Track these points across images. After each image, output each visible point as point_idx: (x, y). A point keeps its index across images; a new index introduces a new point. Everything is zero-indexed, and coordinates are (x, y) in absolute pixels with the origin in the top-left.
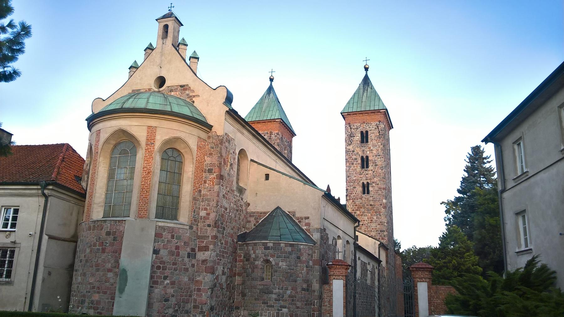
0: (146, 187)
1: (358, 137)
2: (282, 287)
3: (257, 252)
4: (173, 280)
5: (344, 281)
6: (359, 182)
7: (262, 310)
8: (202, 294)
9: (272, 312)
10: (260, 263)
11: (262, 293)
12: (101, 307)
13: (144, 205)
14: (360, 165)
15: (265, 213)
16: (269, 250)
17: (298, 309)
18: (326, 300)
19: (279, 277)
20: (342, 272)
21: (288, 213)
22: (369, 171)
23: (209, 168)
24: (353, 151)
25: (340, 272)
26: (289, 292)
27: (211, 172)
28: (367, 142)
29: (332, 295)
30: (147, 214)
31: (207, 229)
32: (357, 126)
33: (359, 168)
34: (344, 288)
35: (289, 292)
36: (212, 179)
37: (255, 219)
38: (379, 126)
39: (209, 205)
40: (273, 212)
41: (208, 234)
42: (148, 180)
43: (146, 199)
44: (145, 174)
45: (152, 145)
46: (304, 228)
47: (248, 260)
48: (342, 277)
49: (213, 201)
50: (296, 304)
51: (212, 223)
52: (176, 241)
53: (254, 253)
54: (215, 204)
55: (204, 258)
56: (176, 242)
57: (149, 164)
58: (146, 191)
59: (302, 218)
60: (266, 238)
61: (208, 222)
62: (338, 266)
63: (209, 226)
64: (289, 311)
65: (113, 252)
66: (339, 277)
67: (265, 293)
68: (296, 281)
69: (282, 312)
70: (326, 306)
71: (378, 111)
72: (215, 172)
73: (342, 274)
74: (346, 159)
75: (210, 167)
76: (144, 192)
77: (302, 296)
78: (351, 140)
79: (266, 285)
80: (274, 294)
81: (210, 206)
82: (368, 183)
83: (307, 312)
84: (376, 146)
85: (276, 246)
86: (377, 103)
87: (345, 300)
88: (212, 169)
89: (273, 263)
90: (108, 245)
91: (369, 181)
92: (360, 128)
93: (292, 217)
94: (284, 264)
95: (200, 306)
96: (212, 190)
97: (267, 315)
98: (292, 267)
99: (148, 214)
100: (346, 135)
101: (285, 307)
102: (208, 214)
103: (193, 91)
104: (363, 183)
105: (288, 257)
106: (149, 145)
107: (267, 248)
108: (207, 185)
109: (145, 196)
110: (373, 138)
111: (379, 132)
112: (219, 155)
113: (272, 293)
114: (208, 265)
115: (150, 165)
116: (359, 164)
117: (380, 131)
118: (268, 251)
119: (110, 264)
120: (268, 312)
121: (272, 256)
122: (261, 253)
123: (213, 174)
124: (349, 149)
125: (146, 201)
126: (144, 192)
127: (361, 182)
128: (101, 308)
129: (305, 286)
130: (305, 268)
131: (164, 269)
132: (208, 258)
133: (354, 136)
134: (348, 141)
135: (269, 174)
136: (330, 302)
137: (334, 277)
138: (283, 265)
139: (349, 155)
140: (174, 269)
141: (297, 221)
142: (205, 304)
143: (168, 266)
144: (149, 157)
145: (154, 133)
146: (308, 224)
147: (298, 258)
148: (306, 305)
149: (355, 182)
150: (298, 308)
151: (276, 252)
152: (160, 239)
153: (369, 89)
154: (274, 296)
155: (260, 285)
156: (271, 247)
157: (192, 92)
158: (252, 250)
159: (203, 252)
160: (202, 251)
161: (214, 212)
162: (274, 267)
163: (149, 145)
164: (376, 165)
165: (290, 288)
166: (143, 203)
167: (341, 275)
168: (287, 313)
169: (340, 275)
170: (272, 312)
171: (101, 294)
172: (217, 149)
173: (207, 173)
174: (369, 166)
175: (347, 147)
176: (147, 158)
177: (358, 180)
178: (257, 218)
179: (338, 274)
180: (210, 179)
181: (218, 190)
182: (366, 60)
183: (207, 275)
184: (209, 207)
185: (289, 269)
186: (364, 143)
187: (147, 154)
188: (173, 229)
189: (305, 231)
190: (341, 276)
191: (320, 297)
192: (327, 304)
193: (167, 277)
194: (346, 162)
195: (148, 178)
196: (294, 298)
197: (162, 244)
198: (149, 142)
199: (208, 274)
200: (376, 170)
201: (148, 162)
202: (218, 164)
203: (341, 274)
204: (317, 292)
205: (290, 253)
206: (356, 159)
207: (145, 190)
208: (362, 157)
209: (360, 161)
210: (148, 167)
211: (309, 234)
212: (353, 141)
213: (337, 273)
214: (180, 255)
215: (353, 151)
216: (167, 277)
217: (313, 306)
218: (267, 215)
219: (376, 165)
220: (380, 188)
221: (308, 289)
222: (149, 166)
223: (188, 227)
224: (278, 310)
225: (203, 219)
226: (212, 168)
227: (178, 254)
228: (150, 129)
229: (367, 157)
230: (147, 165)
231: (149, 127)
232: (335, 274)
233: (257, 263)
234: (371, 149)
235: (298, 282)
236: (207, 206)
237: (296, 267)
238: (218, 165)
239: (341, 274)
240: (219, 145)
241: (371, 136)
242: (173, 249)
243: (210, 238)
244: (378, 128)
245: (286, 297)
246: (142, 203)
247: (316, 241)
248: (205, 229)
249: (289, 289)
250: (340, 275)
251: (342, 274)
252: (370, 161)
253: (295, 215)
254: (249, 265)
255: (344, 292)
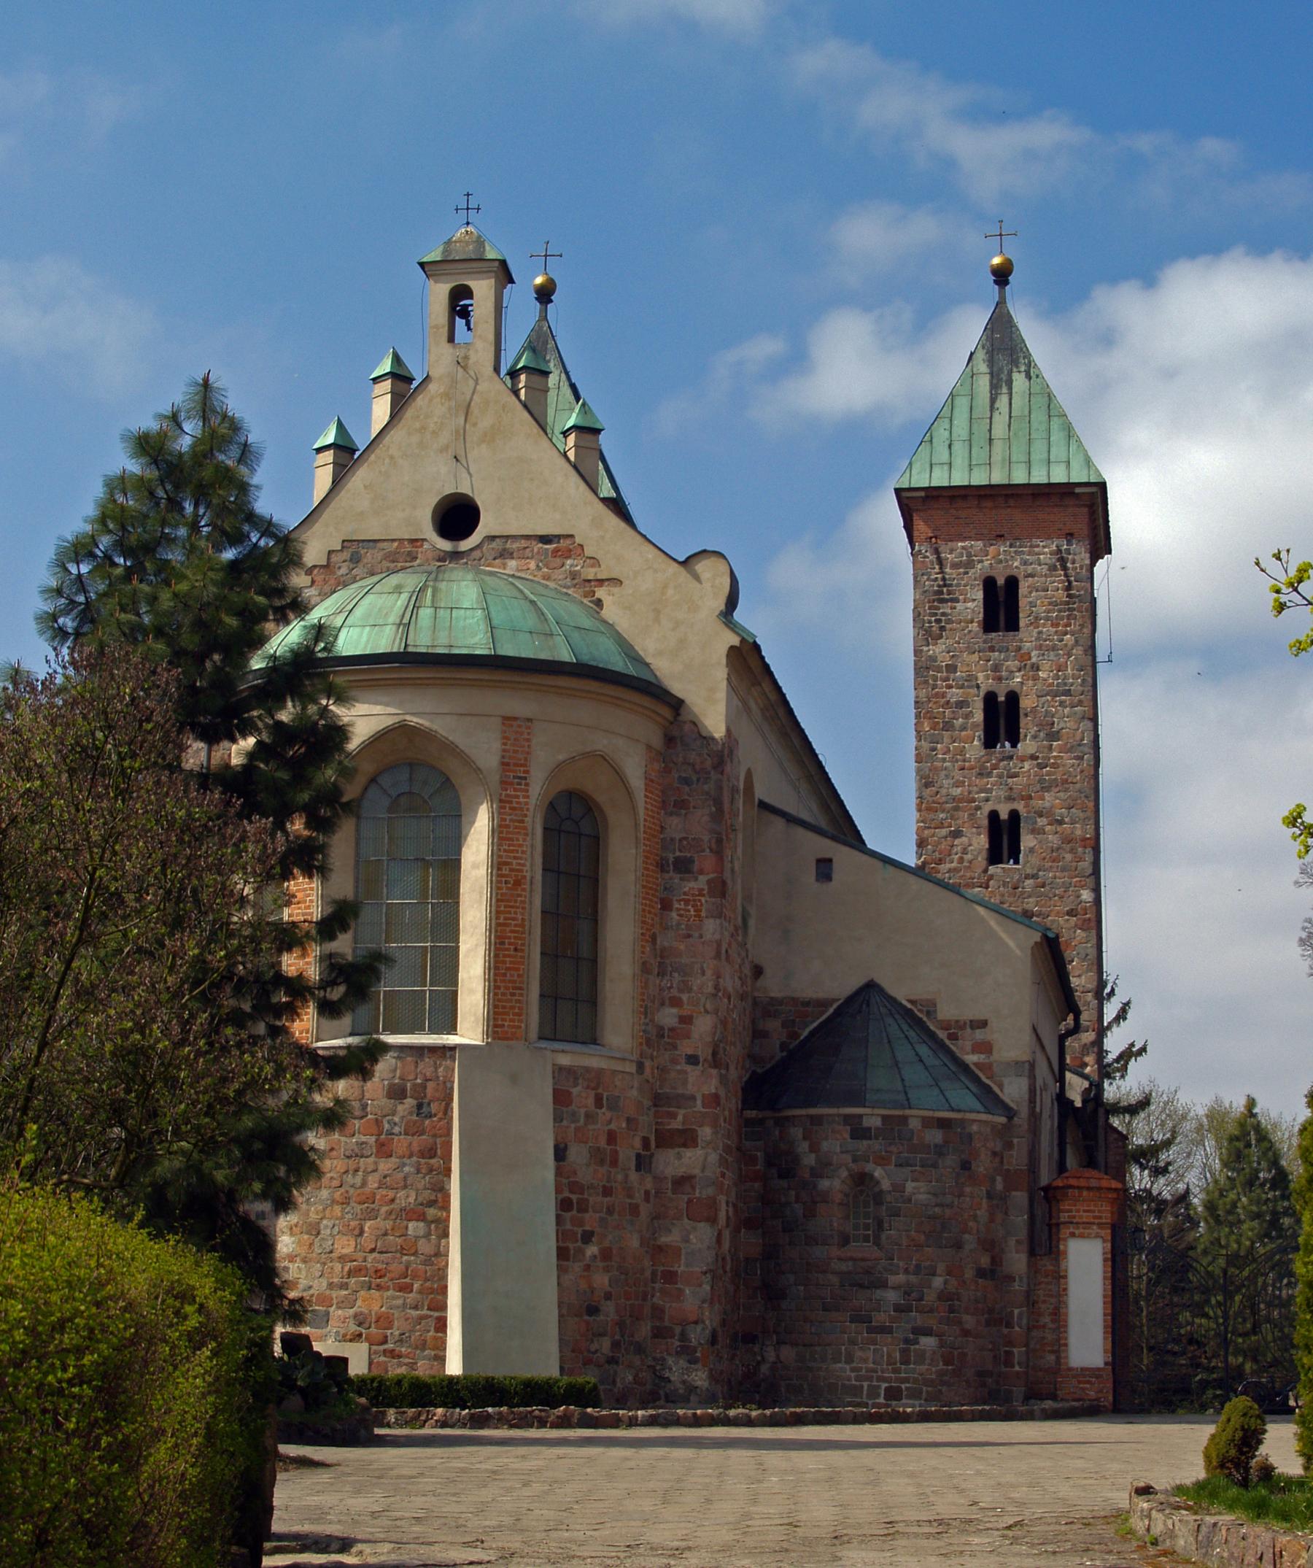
0: (512, 931)
1: (972, 604)
2: (918, 1266)
3: (825, 1146)
4: (606, 1244)
5: (1104, 1241)
6: (978, 808)
7: (853, 1342)
8: (681, 1291)
9: (885, 1349)
10: (837, 1184)
11: (850, 1285)
12: (397, 1333)
13: (512, 994)
14: (980, 733)
15: (823, 1004)
16: (870, 1139)
17: (966, 1336)
18: (1043, 1306)
19: (907, 1231)
20: (1099, 1211)
21: (909, 1006)
22: (1022, 759)
23: (678, 854)
24: (952, 668)
25: (1094, 1212)
26: (938, 1282)
27: (688, 871)
28: (1013, 625)
29: (1065, 1290)
30: (523, 1025)
31: (686, 1072)
32: (969, 555)
33: (975, 748)
34: (1105, 1266)
35: (938, 1282)
36: (693, 895)
37: (784, 1025)
38: (1070, 557)
39: (686, 987)
40: (850, 1000)
41: (690, 1089)
42: (518, 908)
43: (516, 974)
44: (508, 888)
45: (520, 784)
46: (971, 1059)
47: (786, 1173)
48: (1099, 1228)
49: (703, 973)
50: (960, 1322)
51: (704, 1053)
52: (609, 1115)
53: (814, 1148)
54: (710, 984)
55: (681, 1171)
56: (608, 1118)
57: (517, 852)
58: (512, 947)
59: (961, 1025)
60: (856, 1097)
61: (686, 1048)
62: (1085, 1193)
63: (692, 1060)
64: (942, 1345)
65: (422, 1154)
66: (1089, 1228)
67: (861, 1286)
68: (958, 1246)
69: (917, 1347)
70: (1044, 1326)
71: (1064, 492)
72: (701, 872)
73: (1100, 1218)
74: (916, 702)
75: (680, 851)
76: (508, 950)
77: (979, 1294)
78: (944, 614)
79: (863, 1260)
80: (893, 1288)
81: (690, 990)
82: (1014, 815)
83: (990, 1347)
84: (1054, 648)
85: (894, 1127)
86: (1058, 452)
87: (1109, 1306)
88: (691, 861)
89: (886, 1185)
90: (396, 1130)
91: (1020, 806)
92: (981, 561)
93: (925, 1019)
94: (922, 1186)
95: (678, 1330)
96: (696, 934)
97: (868, 1358)
98: (948, 1199)
99: (526, 1026)
100: (919, 591)
101: (928, 1332)
102: (686, 1020)
103: (595, 562)
104: (993, 815)
105: (935, 1166)
106: (512, 784)
107: (859, 1132)
108: (674, 914)
109: (511, 962)
110: (1041, 610)
111: (1069, 588)
112: (714, 809)
113: (883, 1285)
114: (697, 1195)
115: (519, 855)
116: (975, 726)
117: (1075, 583)
118: (865, 1142)
119: (413, 1194)
120: (872, 1347)
121: (882, 1161)
122: (838, 1150)
123: (696, 879)
124: (933, 659)
125: (514, 982)
126: (508, 950)
127: (987, 808)
128: (397, 1338)
129: (985, 1261)
130: (984, 1200)
131: (583, 1208)
132: (697, 1171)
133: (957, 601)
134: (930, 622)
135: (830, 860)
136: (1056, 1314)
137: (1072, 1230)
138: (918, 1190)
139: (934, 687)
140: (608, 1208)
141: (942, 1035)
142: (696, 1323)
143: (591, 1199)
144: (516, 827)
145: (525, 739)
146: (985, 1047)
147: (966, 1166)
148: (988, 1323)
149: (956, 809)
150: (966, 1333)
151: (894, 1149)
152: (565, 1109)
153: (1019, 380)
154: (891, 1296)
155: (840, 1259)
156: (877, 1129)
157: (593, 566)
158: (804, 1138)
159: (677, 1150)
160: (672, 1146)
161: (707, 1012)
162: (888, 1200)
163: (512, 784)
164: (1053, 736)
165: (941, 1268)
166: (507, 988)
167: (1096, 1221)
168: (934, 1353)
169: (1094, 1223)
170: (885, 1349)
171: (390, 1293)
172: (706, 787)
173: (671, 873)
174: (1022, 736)
175: (925, 649)
176: (508, 833)
177: (973, 800)
178: (793, 1021)
179: (1085, 1220)
180: (685, 894)
181: (717, 937)
182: (1001, 235)
183: (695, 1229)
184: (687, 995)
185: (937, 1205)
186: (996, 630)
187: (508, 818)
188: (600, 1072)
189: (973, 1072)
190: (1095, 1227)
191: (1030, 1301)
192: (1046, 1319)
193: (592, 1234)
194: (918, 716)
195: (516, 901)
196: (956, 1302)
197: (573, 1125)
198: (512, 774)
199: (702, 1224)
200: (1055, 757)
201: (513, 845)
202: (714, 841)
203: (1095, 1217)
204: (1021, 1280)
205: (940, 1151)
206: (961, 704)
207: (510, 944)
208: (990, 699)
209: (979, 716)
210: (514, 862)
211: (987, 1081)
212: (949, 622)
213: (1081, 1217)
214: (620, 1161)
215: (952, 668)
216: (592, 1234)
217: (1006, 1327)
218: (831, 1010)
219: (1053, 736)
220: (1068, 840)
221: (993, 1273)
222: (515, 858)
223: (632, 1068)
224: (907, 1341)
225: (669, 1037)
226: (689, 855)
227: (614, 1163)
228: (512, 726)
229: (1013, 698)
230: (510, 857)
231: (508, 720)
232: (1075, 1221)
233: (824, 1184)
234: (1034, 660)
235: (967, 1247)
236: (680, 991)
237: (959, 1196)
238: (714, 846)
239: (1095, 1217)
240: (712, 773)
241: (1027, 598)
242: (602, 1143)
243: (699, 1102)
244: (1065, 568)
245: (930, 1297)
246: (507, 988)
247: (1015, 1108)
248: (679, 1072)
249: (939, 1271)
250: (1094, 1223)
251: (1100, 1218)
252: (1026, 715)
253: (935, 1011)
254: (793, 1193)
255: (1105, 1278)
